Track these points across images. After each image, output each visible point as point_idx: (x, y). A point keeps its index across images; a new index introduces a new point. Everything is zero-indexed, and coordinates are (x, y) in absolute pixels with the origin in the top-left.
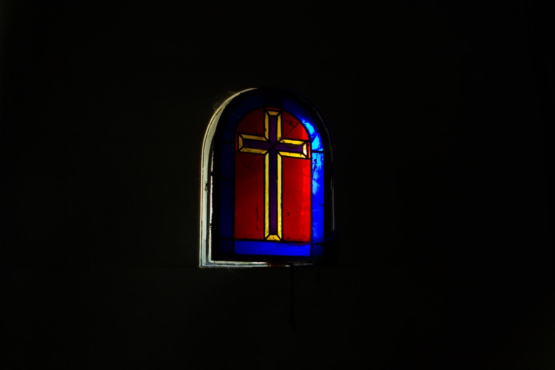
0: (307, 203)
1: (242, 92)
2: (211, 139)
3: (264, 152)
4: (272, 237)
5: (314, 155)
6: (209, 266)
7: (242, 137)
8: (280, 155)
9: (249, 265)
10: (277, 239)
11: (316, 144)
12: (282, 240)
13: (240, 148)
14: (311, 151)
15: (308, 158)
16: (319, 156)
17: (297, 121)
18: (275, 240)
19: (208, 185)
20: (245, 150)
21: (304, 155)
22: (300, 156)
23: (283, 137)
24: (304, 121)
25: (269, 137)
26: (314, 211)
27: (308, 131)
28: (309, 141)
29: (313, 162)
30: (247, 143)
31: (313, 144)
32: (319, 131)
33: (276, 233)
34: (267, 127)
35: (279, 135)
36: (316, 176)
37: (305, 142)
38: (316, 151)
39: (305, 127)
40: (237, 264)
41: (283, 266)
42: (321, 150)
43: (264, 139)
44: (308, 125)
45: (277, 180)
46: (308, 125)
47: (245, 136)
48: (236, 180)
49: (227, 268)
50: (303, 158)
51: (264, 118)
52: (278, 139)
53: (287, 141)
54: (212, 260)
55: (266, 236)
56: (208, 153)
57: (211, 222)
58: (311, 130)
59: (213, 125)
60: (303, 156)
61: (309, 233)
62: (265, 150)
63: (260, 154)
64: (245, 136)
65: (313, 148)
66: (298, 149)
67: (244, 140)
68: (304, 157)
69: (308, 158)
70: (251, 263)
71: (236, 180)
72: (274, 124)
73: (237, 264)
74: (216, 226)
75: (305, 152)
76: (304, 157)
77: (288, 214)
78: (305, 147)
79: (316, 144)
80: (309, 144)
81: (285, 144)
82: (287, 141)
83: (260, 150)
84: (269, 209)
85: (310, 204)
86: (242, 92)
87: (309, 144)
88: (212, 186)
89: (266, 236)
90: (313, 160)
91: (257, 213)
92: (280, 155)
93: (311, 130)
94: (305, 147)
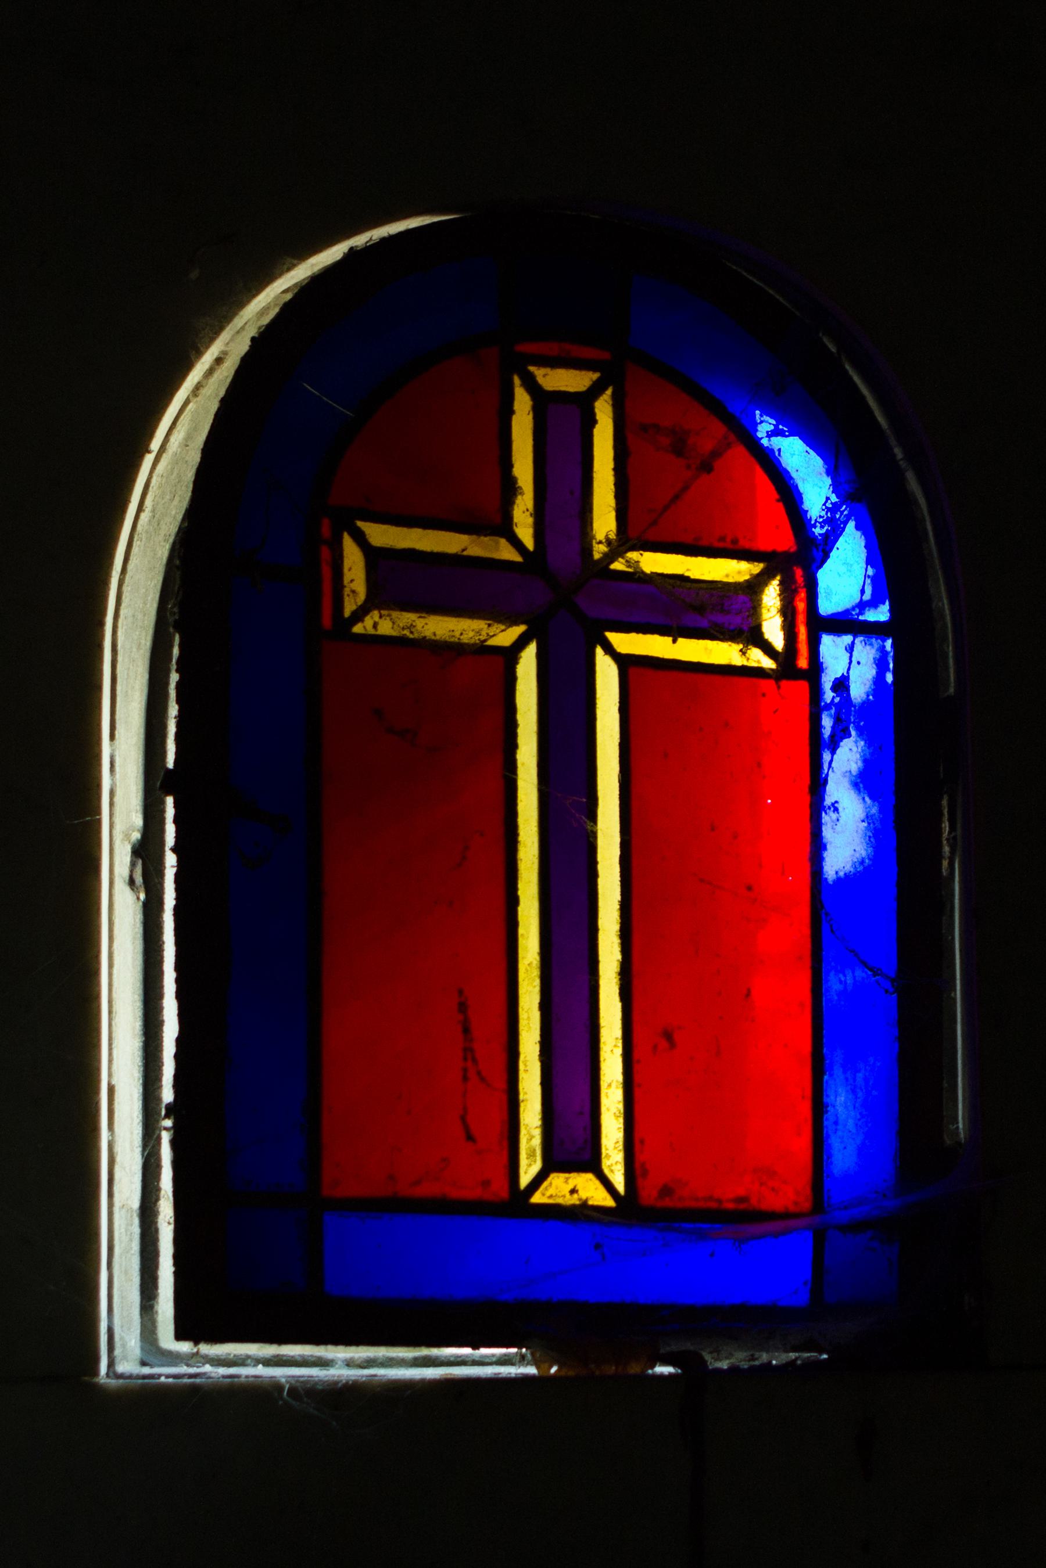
0: (789, 932)
1: (360, 240)
2: (163, 552)
3: (506, 636)
4: (563, 1189)
5: (833, 651)
6: (165, 1372)
7: (360, 539)
8: (609, 649)
9: (418, 1363)
10: (601, 1198)
11: (844, 576)
12: (628, 1204)
13: (349, 608)
14: (810, 622)
15: (797, 668)
16: (866, 653)
17: (718, 429)
18: (584, 1205)
19: (147, 851)
20: (383, 624)
21: (767, 649)
22: (738, 661)
23: (629, 537)
24: (765, 426)
25: (538, 535)
26: (834, 983)
27: (789, 494)
28: (799, 559)
29: (829, 695)
30: (401, 580)
31: (826, 576)
32: (864, 491)
33: (589, 1161)
34: (523, 470)
35: (604, 522)
36: (847, 757)
37: (775, 564)
38: (843, 623)
39: (770, 462)
40: (342, 1363)
41: (634, 1369)
42: (881, 614)
43: (507, 553)
44: (796, 455)
45: (593, 817)
46: (796, 455)
47: (381, 535)
48: (319, 812)
49: (274, 1387)
50: (758, 672)
51: (507, 411)
52: (599, 550)
53: (656, 563)
54: (179, 1336)
55: (525, 1180)
56: (147, 642)
57: (168, 1095)
58: (816, 492)
59: (176, 461)
60: (758, 658)
61: (802, 1145)
62: (511, 621)
63: (483, 650)
64: (382, 535)
65: (827, 606)
66: (725, 613)
67: (373, 556)
68: (768, 663)
69: (797, 668)
70: (435, 1352)
71: (319, 812)
72: (568, 446)
73: (342, 1363)
74: (201, 1119)
75: (773, 630)
76: (768, 663)
77: (668, 1036)
78: (771, 596)
79: (844, 576)
80: (799, 573)
81: (637, 577)
82: (656, 563)
83: (480, 624)
84: (545, 1006)
85: (807, 931)
86: (360, 240)
87: (799, 573)
88: (171, 860)
89: (525, 1180)
90: (827, 682)
91: (466, 1030)
92: (609, 649)
93: (816, 492)
94: (771, 596)
